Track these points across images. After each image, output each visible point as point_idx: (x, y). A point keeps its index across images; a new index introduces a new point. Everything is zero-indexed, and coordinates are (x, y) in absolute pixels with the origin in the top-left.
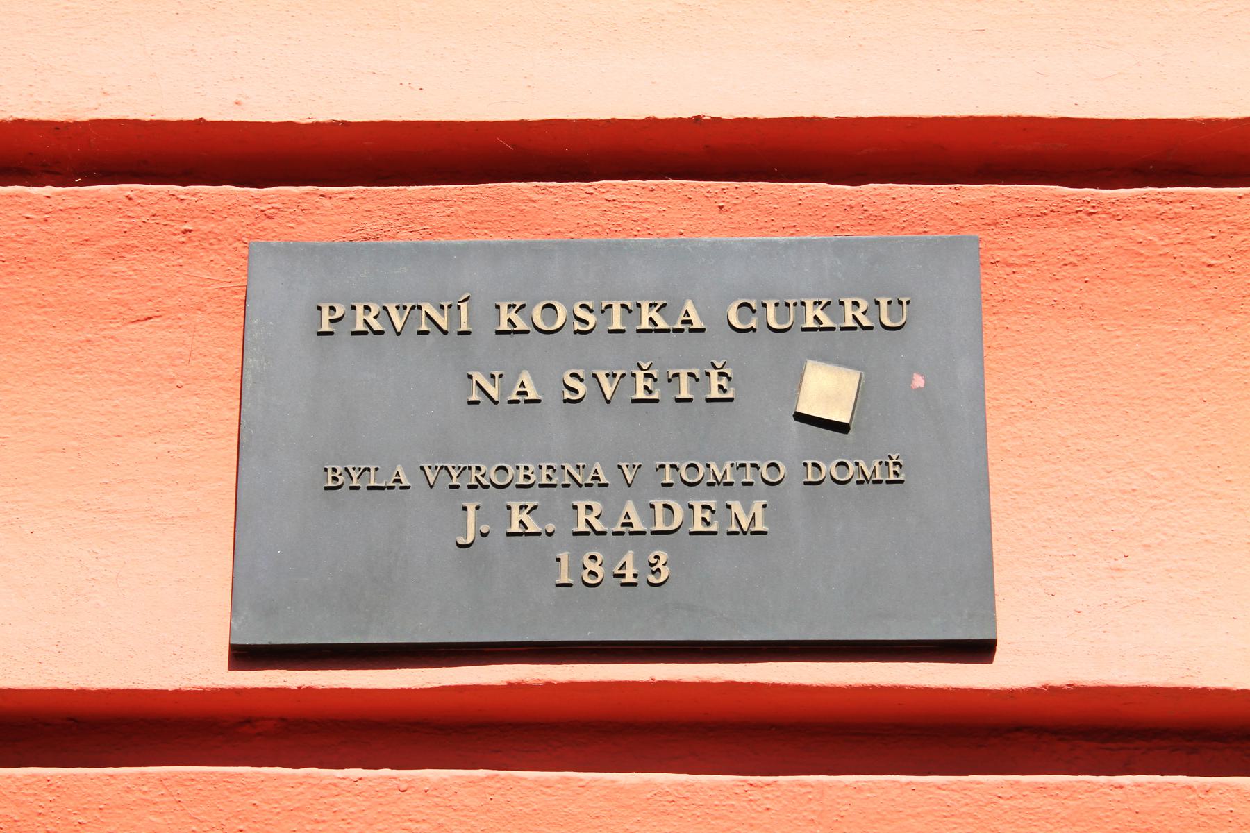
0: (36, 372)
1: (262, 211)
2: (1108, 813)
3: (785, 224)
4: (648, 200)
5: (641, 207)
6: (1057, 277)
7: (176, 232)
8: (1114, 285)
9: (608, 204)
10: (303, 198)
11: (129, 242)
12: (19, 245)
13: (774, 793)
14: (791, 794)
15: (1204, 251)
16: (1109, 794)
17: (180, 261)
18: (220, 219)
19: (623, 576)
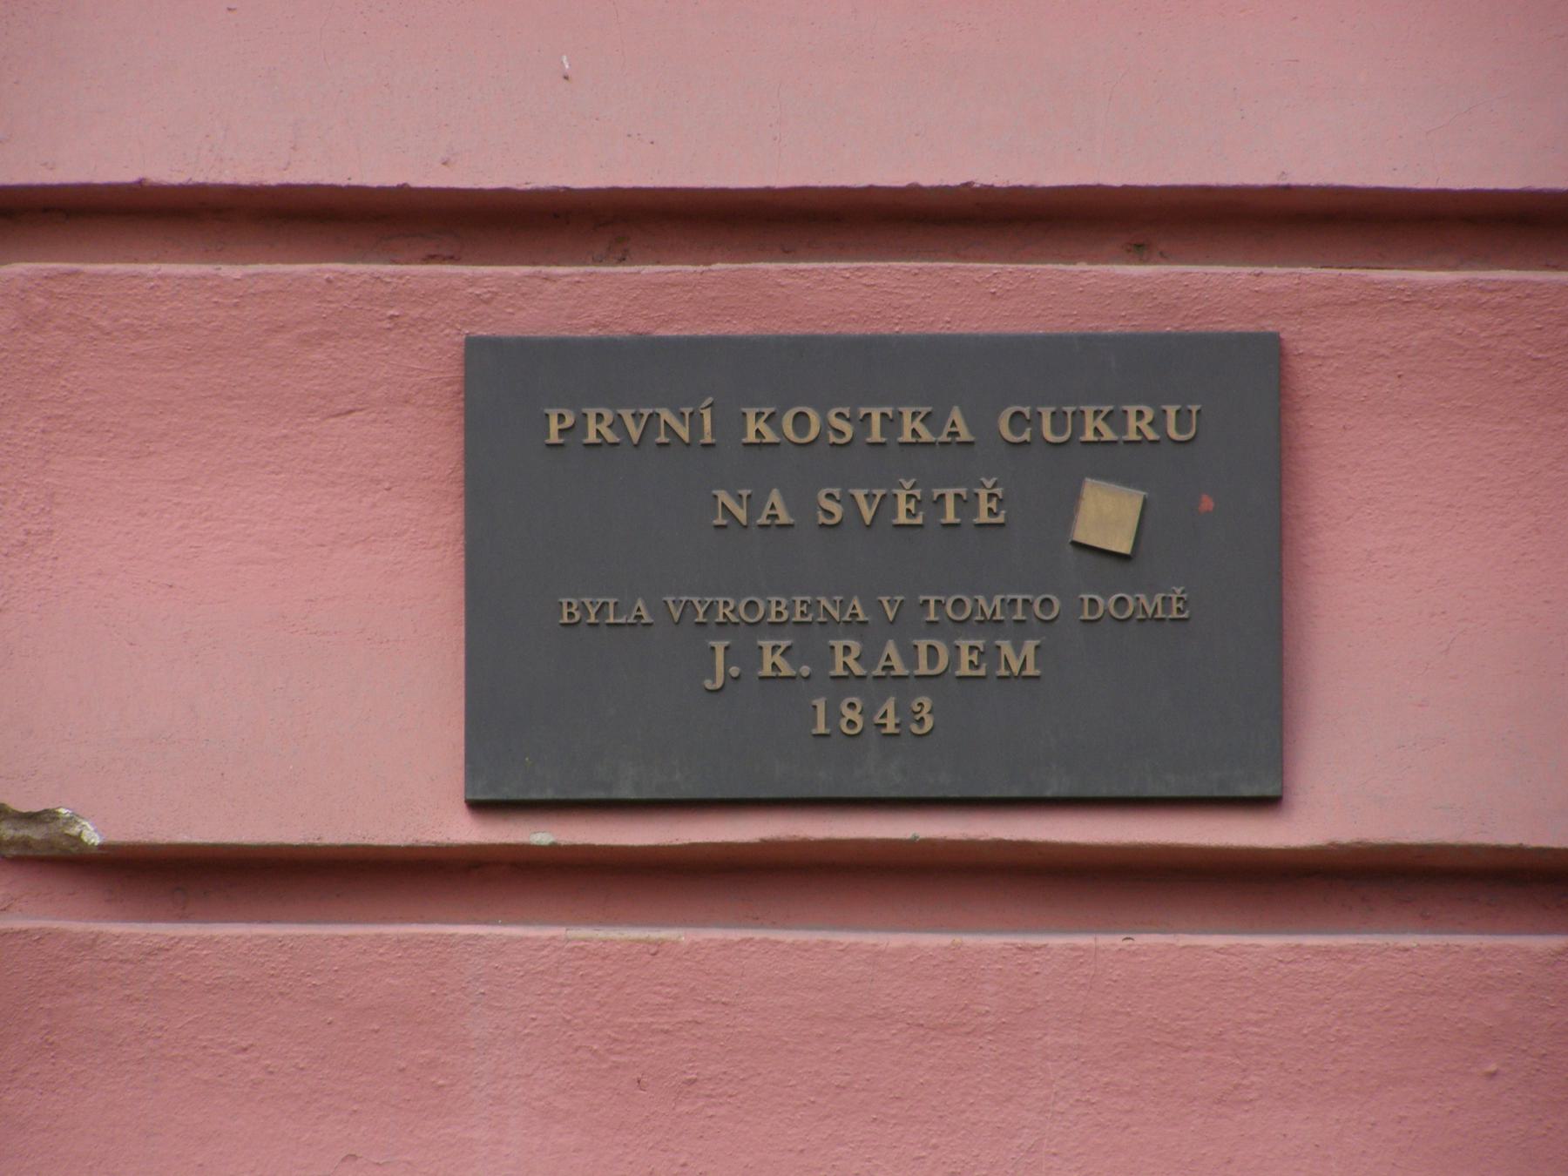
0: (227, 472)
1: (478, 295)
2: (1393, 977)
3: (1063, 312)
4: (911, 285)
5: (903, 293)
6: (1367, 370)
7: (381, 318)
8: (1430, 380)
9: (865, 289)
10: (524, 281)
11: (328, 329)
12: (206, 333)
13: (1043, 956)
14: (1062, 958)
15: (1529, 344)
16: (1393, 958)
17: (386, 349)
18: (430, 303)
19: (884, 725)
